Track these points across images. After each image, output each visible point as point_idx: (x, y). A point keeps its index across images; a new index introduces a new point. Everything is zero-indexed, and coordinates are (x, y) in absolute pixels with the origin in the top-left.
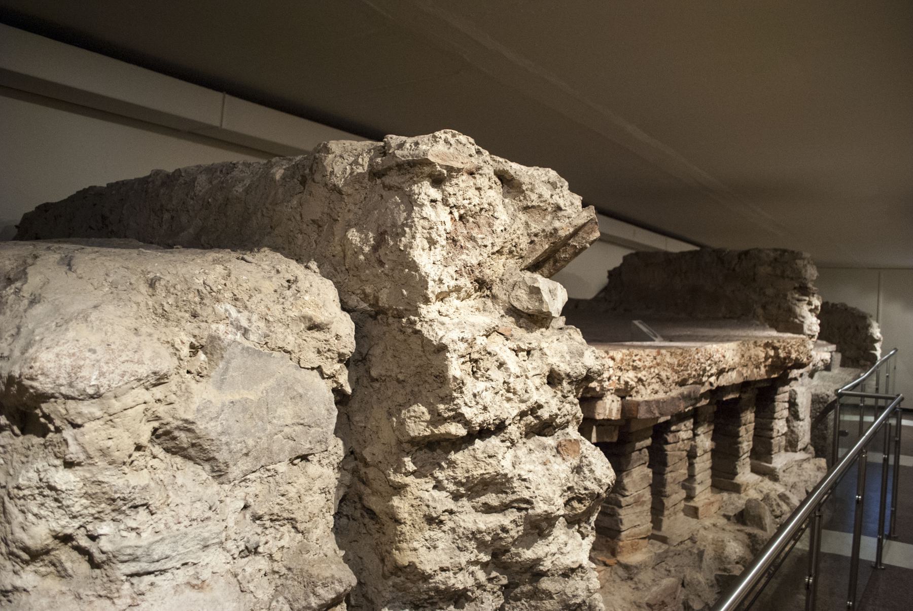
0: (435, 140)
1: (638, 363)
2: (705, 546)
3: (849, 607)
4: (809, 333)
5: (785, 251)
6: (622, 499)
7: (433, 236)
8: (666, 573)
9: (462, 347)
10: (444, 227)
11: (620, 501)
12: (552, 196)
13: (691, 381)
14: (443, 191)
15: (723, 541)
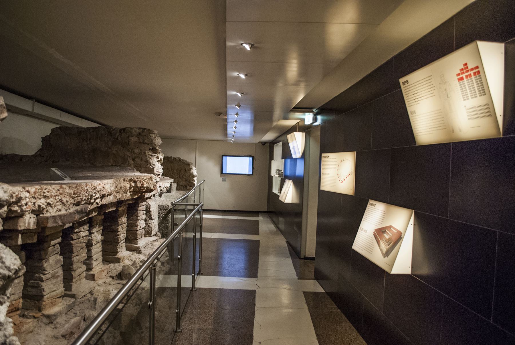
1: (47, 194)
2: (98, 295)
3: (177, 313)
4: (157, 173)
5: (145, 129)
8: (74, 315)
11: (42, 278)
13: (83, 203)
15: (109, 291)
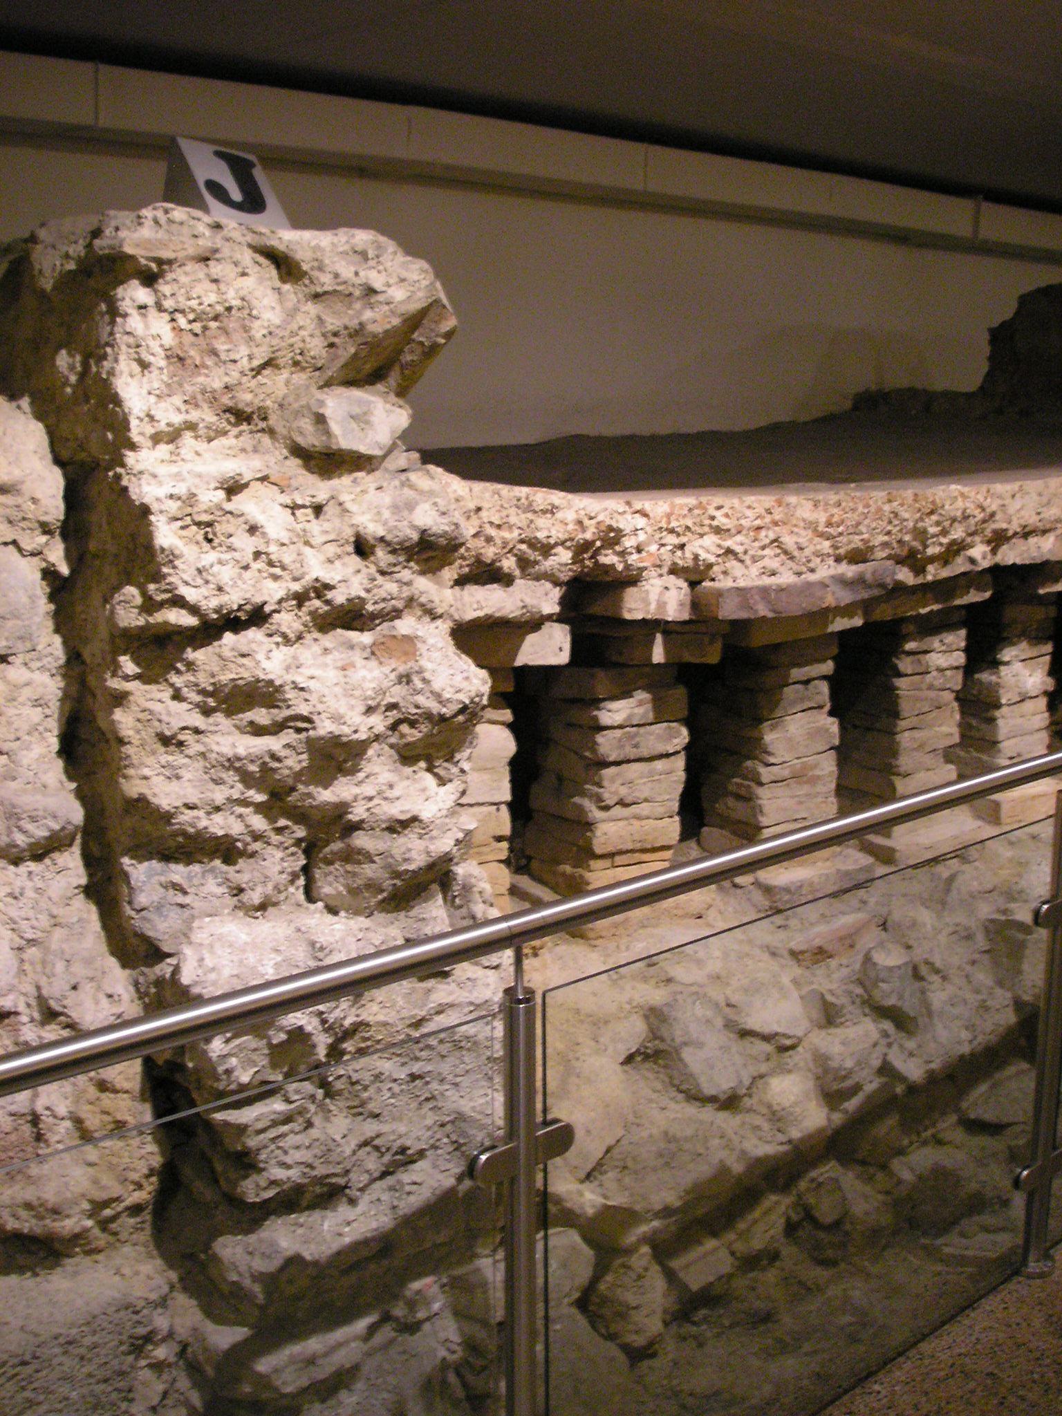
0: (139, 221)
1: (721, 520)
6: (762, 770)
7: (143, 356)
8: (858, 905)
9: (173, 507)
10: (158, 342)
11: (758, 774)
12: (357, 274)
14: (156, 291)
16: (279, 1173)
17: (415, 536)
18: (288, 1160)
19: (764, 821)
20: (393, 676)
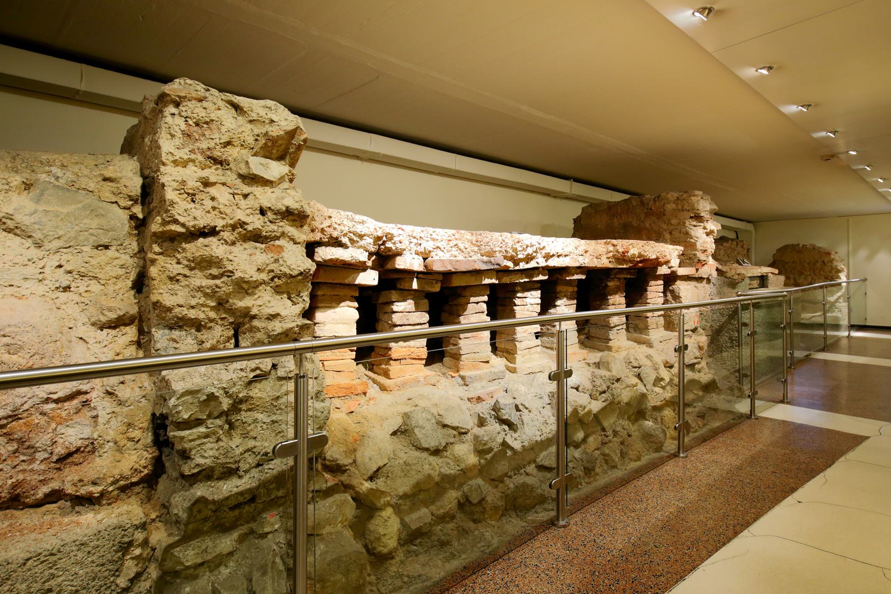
1: (434, 236)
16: (201, 461)
17: (284, 209)
18: (206, 455)
19: (462, 352)
20: (272, 260)
